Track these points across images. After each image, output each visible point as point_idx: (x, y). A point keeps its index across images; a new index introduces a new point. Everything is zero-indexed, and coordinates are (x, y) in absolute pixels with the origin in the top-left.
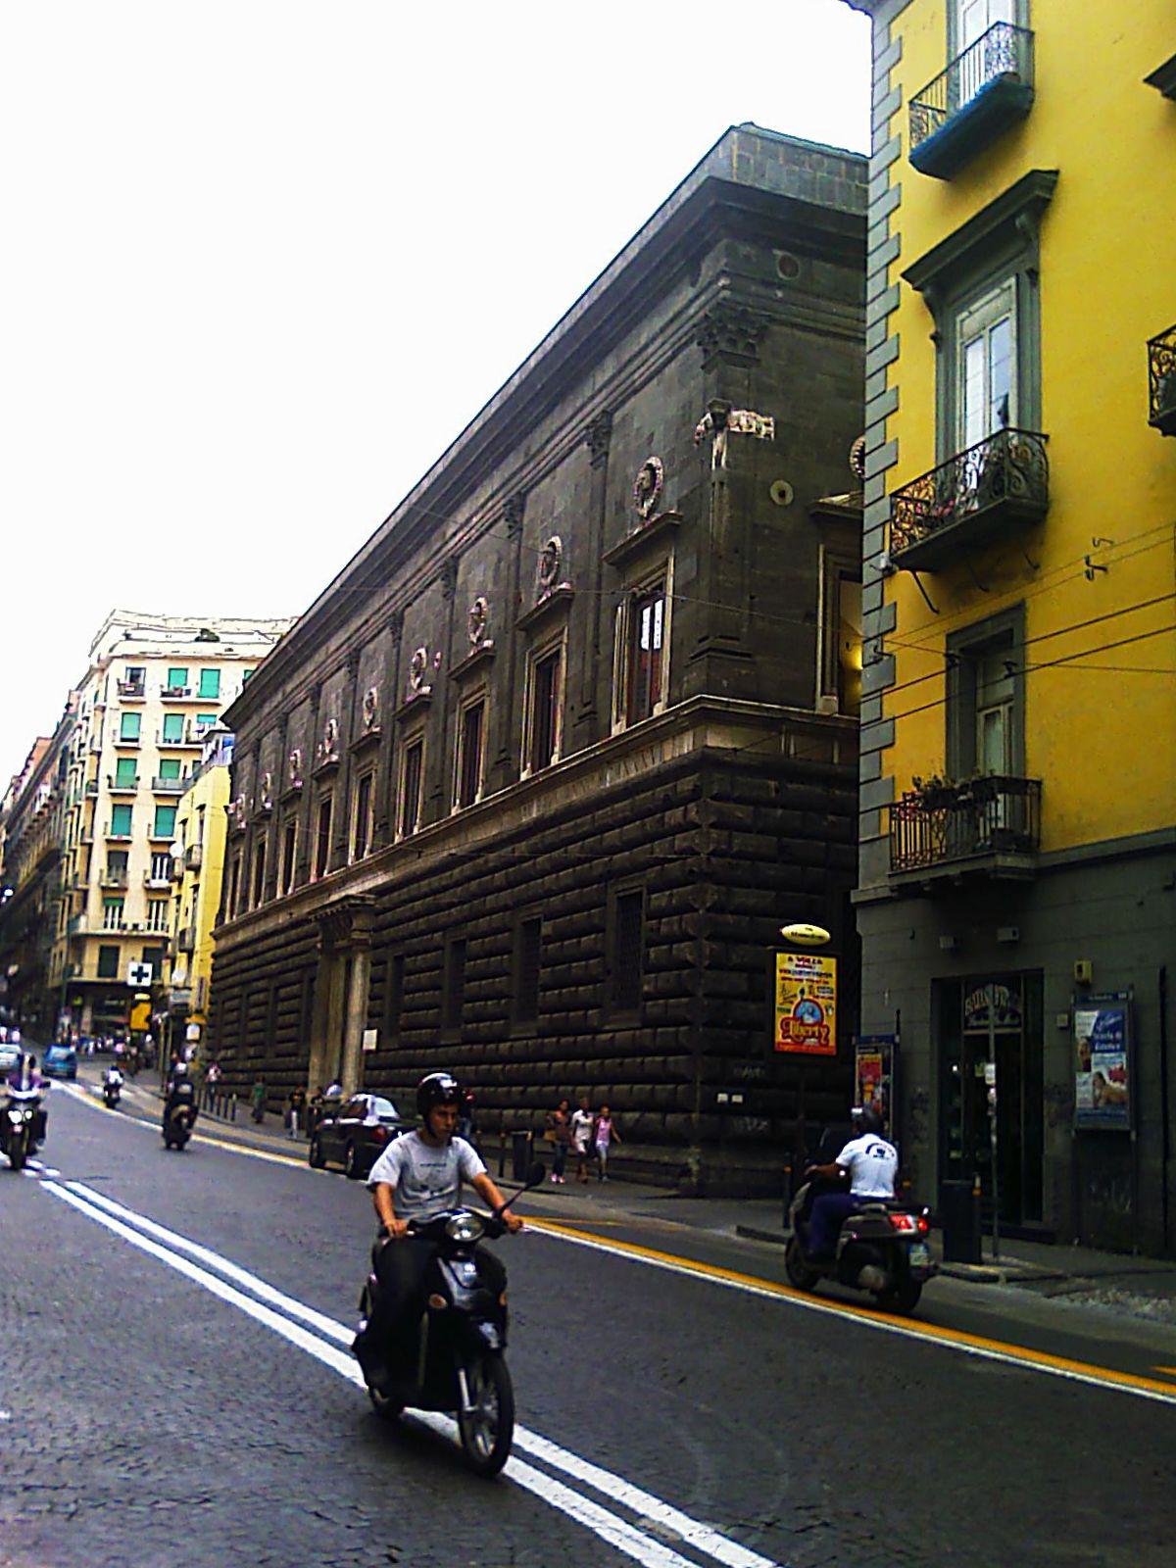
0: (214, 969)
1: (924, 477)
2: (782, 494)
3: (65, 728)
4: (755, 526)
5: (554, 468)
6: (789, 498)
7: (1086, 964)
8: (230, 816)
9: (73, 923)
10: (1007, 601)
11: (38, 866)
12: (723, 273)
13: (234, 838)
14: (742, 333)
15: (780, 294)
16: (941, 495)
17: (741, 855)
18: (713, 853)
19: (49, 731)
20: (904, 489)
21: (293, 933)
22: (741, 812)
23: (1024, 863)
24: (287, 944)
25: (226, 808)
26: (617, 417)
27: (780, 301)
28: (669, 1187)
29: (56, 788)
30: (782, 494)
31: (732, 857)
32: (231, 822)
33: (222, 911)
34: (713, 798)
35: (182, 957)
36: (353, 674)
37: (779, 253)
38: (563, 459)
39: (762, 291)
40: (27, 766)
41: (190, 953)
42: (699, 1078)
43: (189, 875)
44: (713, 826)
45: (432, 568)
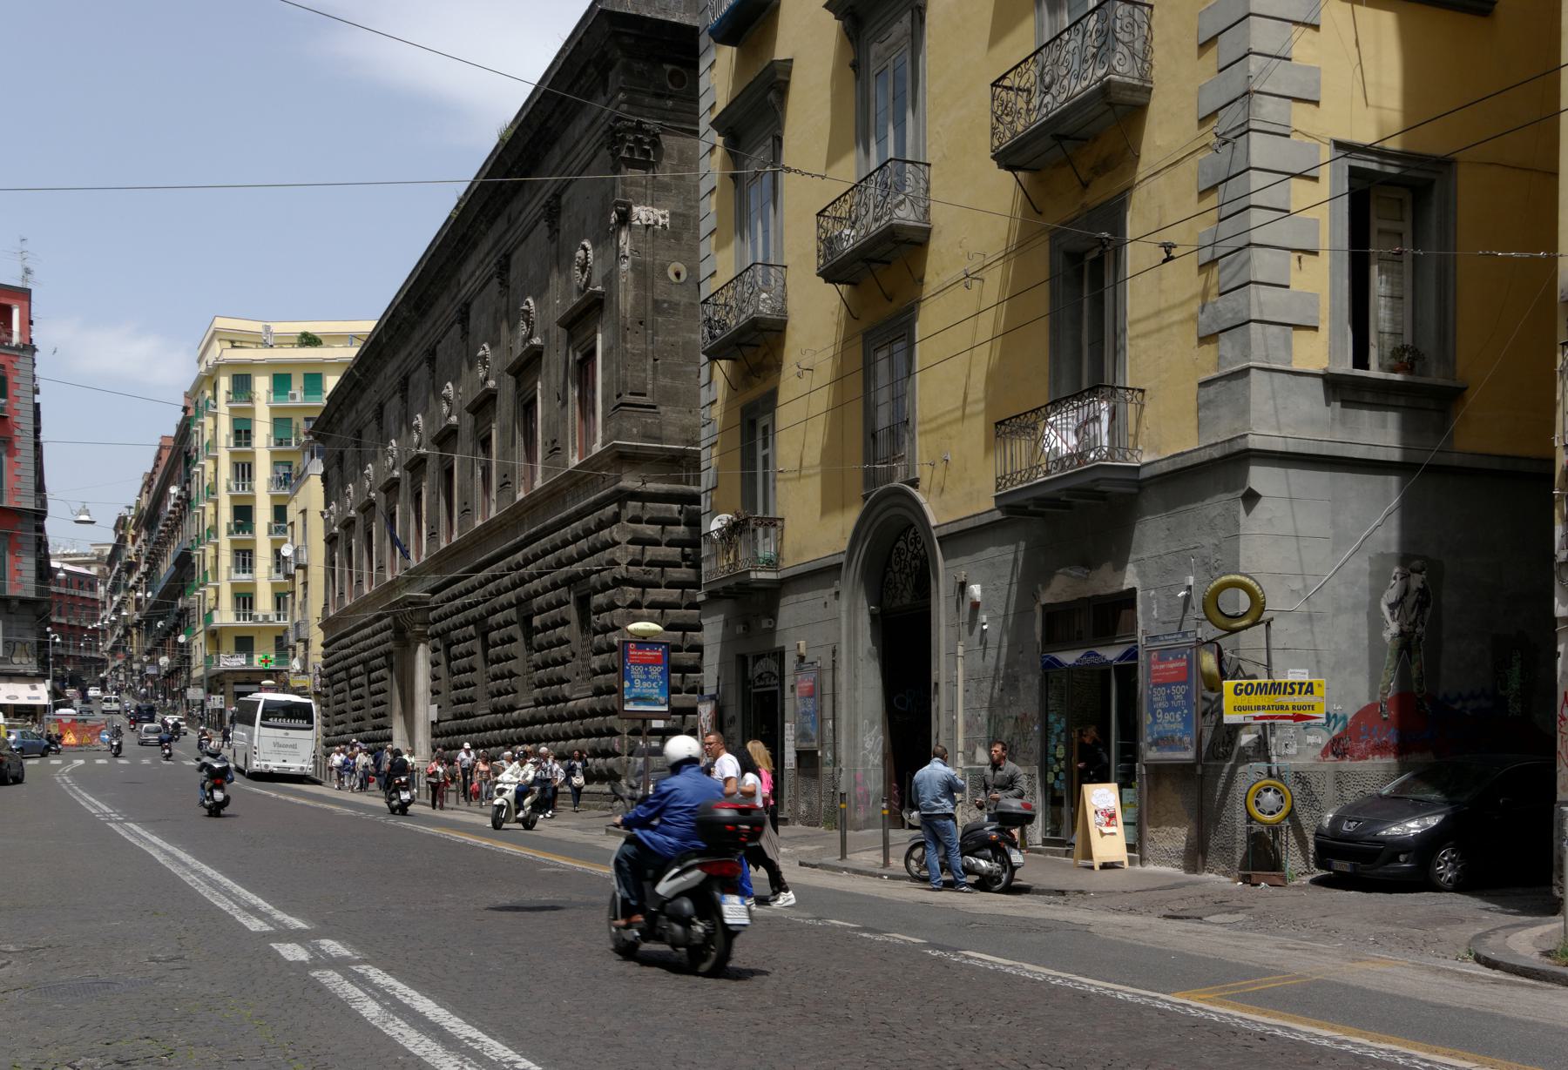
0: (325, 656)
1: (1026, 60)
2: (678, 275)
3: (185, 430)
4: (655, 302)
5: (526, 237)
6: (683, 277)
7: (802, 643)
8: (327, 520)
9: (208, 617)
10: (1116, 188)
11: (175, 563)
12: (621, 89)
13: (331, 540)
14: (639, 142)
15: (670, 103)
16: (1042, 80)
17: (652, 563)
18: (630, 564)
19: (173, 432)
20: (1004, 77)
21: (377, 626)
22: (651, 530)
23: (772, 576)
24: (374, 634)
25: (322, 514)
26: (564, 199)
27: (672, 110)
28: (605, 809)
29: (184, 489)
30: (678, 275)
31: (648, 564)
32: (328, 525)
33: (326, 604)
34: (630, 521)
35: (300, 647)
36: (404, 399)
37: (668, 67)
38: (531, 231)
39: (654, 102)
40: (156, 466)
41: (306, 642)
42: (626, 730)
43: (300, 573)
44: (630, 542)
45: (452, 312)
